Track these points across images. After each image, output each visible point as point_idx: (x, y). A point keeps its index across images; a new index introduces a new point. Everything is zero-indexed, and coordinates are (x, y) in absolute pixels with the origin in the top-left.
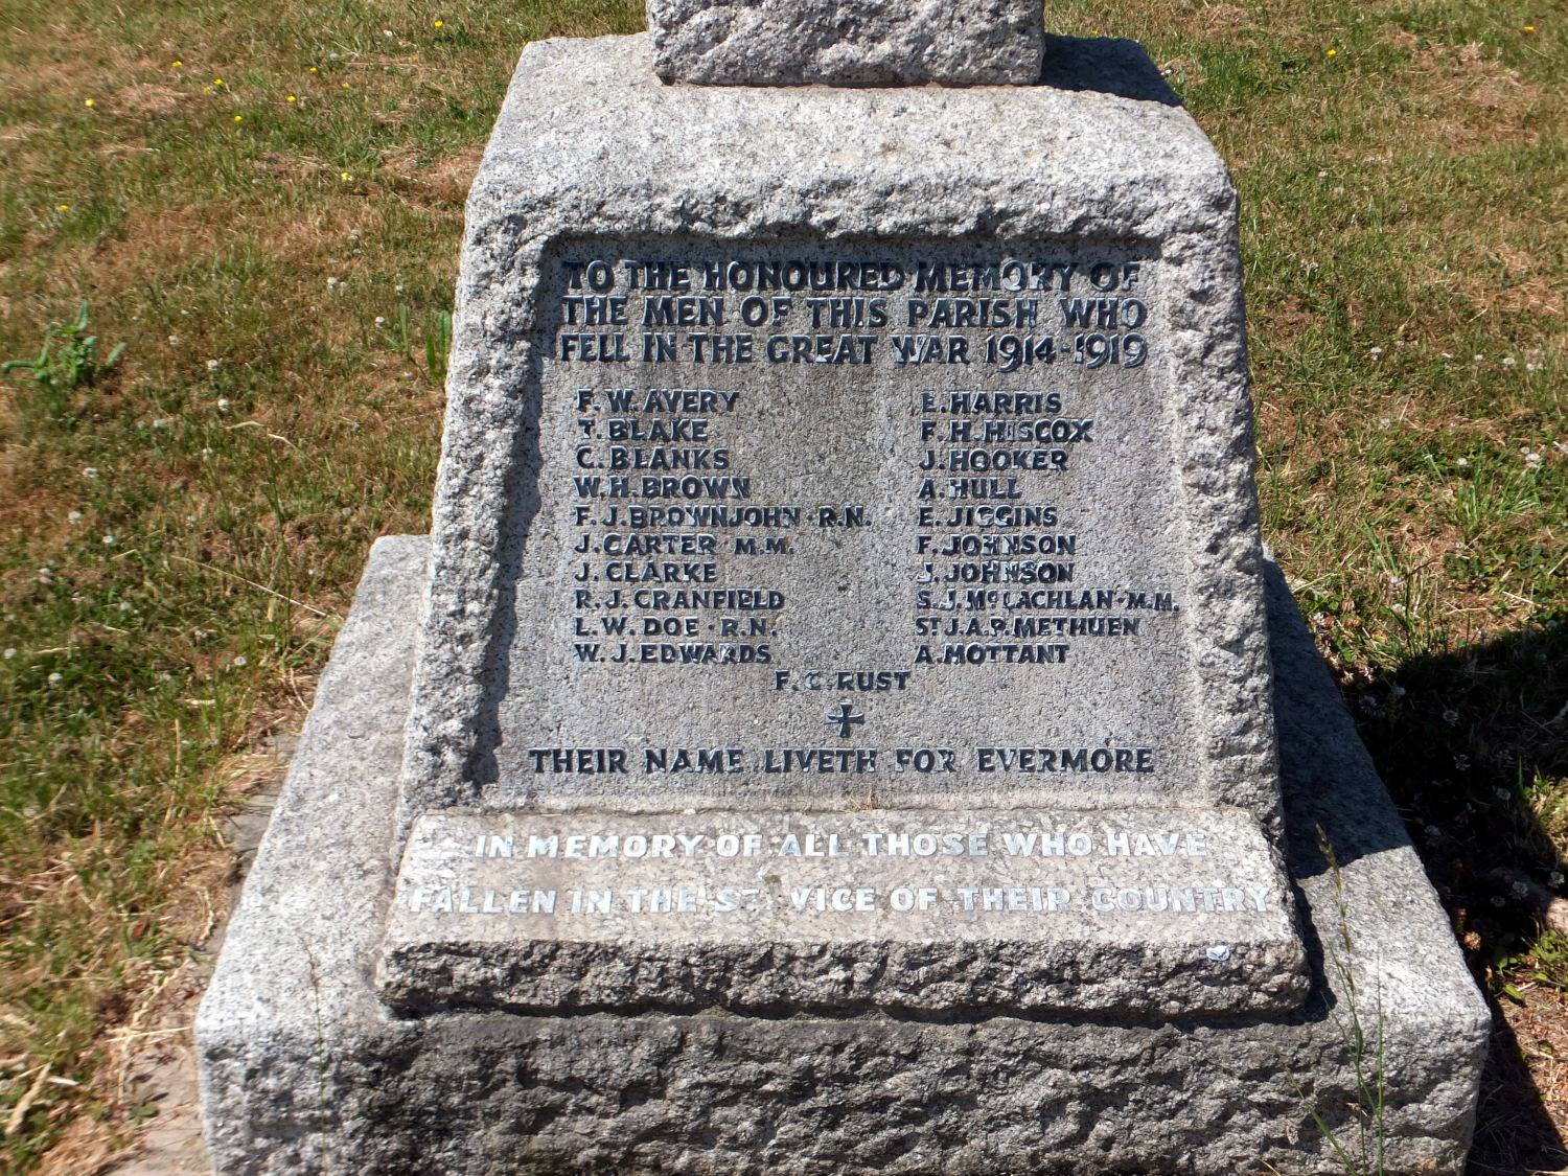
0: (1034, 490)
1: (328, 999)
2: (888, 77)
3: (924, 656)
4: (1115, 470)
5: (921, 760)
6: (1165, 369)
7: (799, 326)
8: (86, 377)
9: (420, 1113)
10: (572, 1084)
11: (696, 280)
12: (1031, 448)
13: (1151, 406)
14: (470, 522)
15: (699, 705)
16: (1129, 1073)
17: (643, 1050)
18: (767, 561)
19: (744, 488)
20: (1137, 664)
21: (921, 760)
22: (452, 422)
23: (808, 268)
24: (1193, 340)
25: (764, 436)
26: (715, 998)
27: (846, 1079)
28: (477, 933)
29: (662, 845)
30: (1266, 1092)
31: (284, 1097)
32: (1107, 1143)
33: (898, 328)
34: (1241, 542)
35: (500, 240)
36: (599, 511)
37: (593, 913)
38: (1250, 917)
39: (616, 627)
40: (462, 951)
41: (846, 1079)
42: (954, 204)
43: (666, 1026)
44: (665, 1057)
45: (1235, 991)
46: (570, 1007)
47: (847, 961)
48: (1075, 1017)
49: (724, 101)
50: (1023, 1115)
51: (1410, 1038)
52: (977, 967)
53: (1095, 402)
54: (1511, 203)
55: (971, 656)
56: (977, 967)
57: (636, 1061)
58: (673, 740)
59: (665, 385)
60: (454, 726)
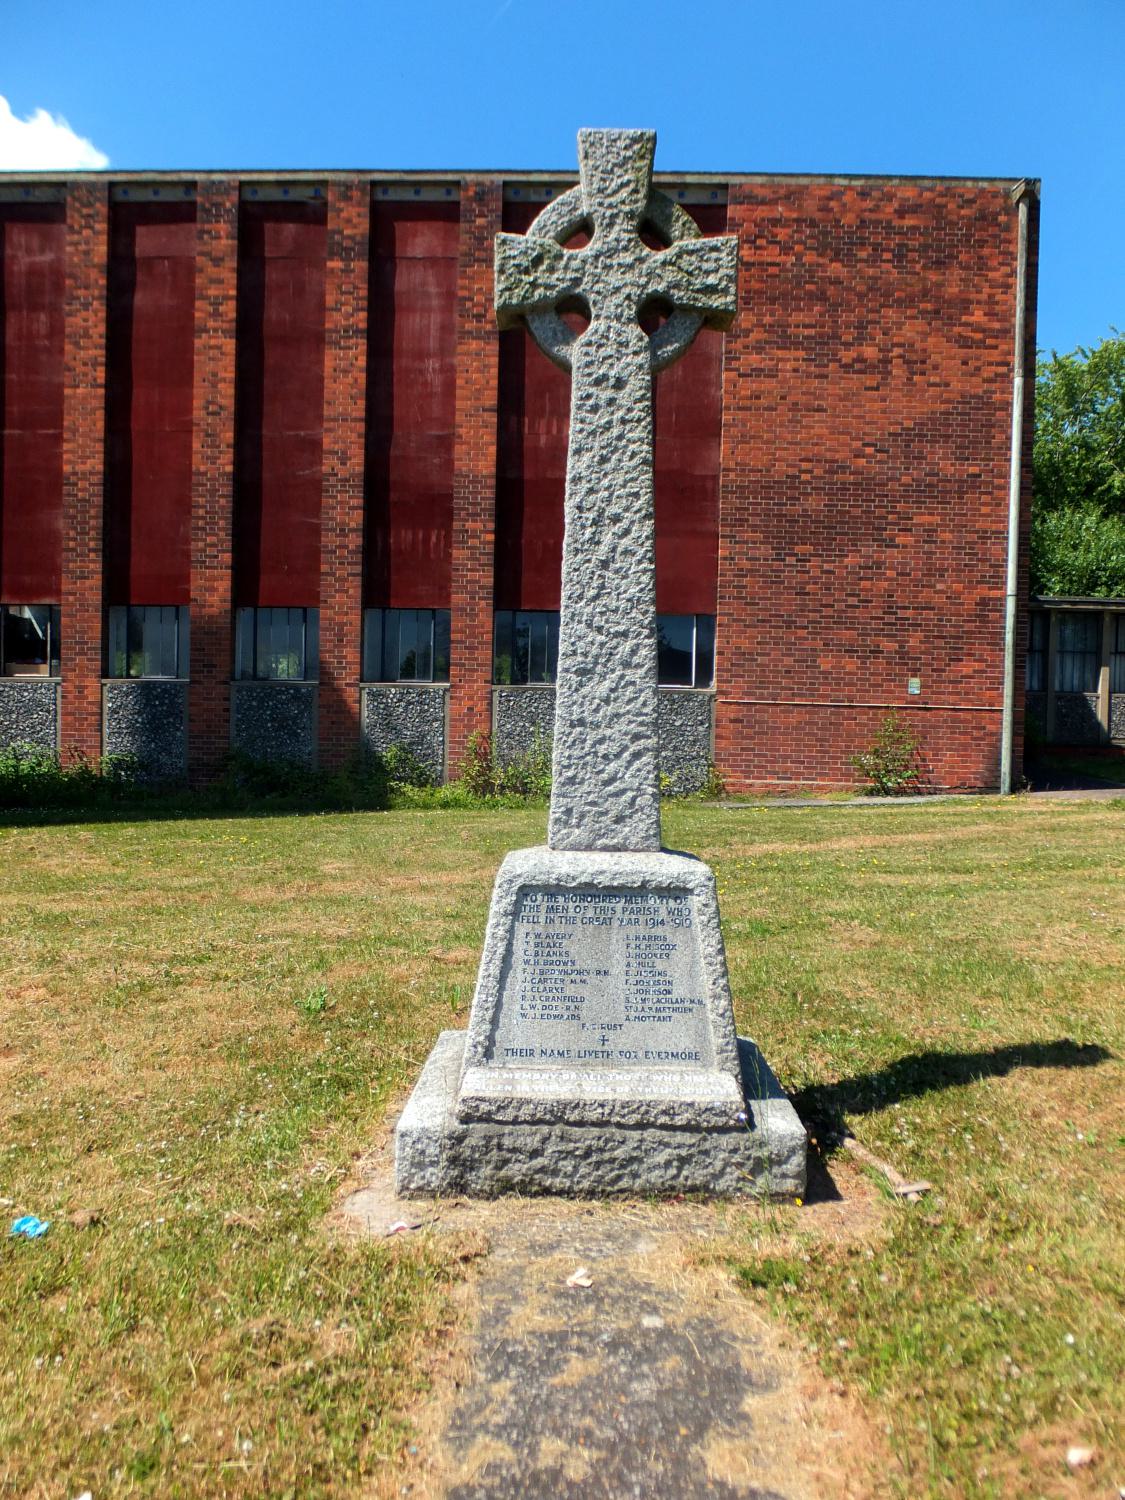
0: (660, 965)
1: (439, 1120)
2: (616, 849)
3: (628, 1019)
4: (685, 959)
5: (626, 1054)
6: (697, 928)
7: (590, 913)
8: (323, 1007)
9: (465, 1160)
10: (514, 1150)
11: (561, 899)
12: (659, 952)
13: (694, 940)
14: (491, 972)
15: (559, 1034)
16: (693, 1150)
17: (538, 1138)
18: (580, 985)
19: (573, 963)
20: (692, 1022)
21: (626, 1054)
22: (488, 940)
23: (594, 896)
24: (705, 918)
25: (580, 947)
26: (560, 1119)
27: (601, 1150)
28: (488, 1094)
29: (545, 1076)
30: (737, 1158)
31: (423, 1152)
32: (686, 1178)
33: (619, 914)
34: (722, 982)
35: (506, 886)
36: (530, 969)
37: (523, 1090)
38: (728, 1095)
39: (533, 1007)
40: (482, 1100)
41: (601, 1150)
42: (635, 878)
43: (545, 1129)
44: (545, 1140)
45: (724, 1119)
46: (515, 1122)
47: (602, 1106)
48: (673, 1128)
49: (569, 854)
50: (657, 1166)
51: (781, 1138)
52: (643, 1109)
53: (678, 938)
54: (863, 966)
55: (641, 1019)
56: (643, 1109)
57: (534, 1142)
58: (549, 1045)
59: (551, 931)
60: (482, 1038)
